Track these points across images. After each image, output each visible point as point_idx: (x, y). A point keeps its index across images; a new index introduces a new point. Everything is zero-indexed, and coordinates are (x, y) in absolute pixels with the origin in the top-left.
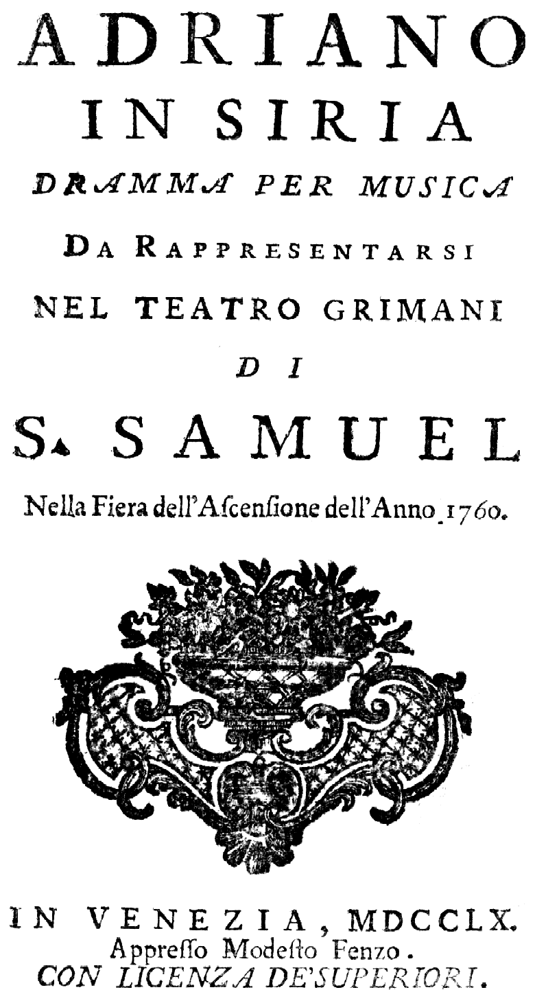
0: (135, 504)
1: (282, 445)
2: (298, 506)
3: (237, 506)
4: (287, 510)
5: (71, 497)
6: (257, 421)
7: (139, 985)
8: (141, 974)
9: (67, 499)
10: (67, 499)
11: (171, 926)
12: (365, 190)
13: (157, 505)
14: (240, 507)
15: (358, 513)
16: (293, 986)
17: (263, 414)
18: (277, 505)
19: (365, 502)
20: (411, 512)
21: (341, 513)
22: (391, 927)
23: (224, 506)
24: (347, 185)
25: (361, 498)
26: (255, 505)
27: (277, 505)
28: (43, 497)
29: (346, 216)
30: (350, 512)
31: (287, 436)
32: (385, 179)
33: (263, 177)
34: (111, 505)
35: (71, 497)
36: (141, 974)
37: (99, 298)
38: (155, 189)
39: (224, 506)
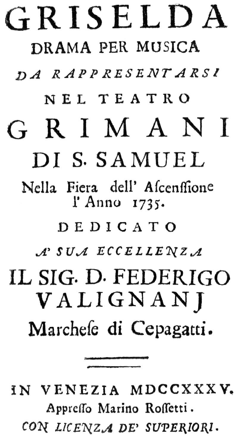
0: (90, 186)
1: (142, 162)
2: (201, 187)
3: (163, 186)
4: (195, 189)
5: (47, 183)
6: (133, 154)
7: (64, 430)
8: (65, 426)
9: (45, 184)
10: (45, 184)
11: (185, 304)
12: (138, 48)
13: (113, 186)
14: (165, 187)
15: (129, 189)
16: (130, 431)
17: (134, 152)
18: (189, 187)
19: (133, 183)
20: (182, 190)
21: (209, 189)
22: (62, 230)
23: (156, 185)
24: (132, 46)
25: (131, 181)
26: (173, 187)
27: (189, 187)
28: (32, 182)
29: (132, 59)
30: (124, 189)
31: (143, 160)
32: (147, 154)
33: (82, 70)
34: (77, 186)
35: (47, 183)
36: (65, 426)
37: (86, 284)
38: (93, 71)
39: (156, 185)
